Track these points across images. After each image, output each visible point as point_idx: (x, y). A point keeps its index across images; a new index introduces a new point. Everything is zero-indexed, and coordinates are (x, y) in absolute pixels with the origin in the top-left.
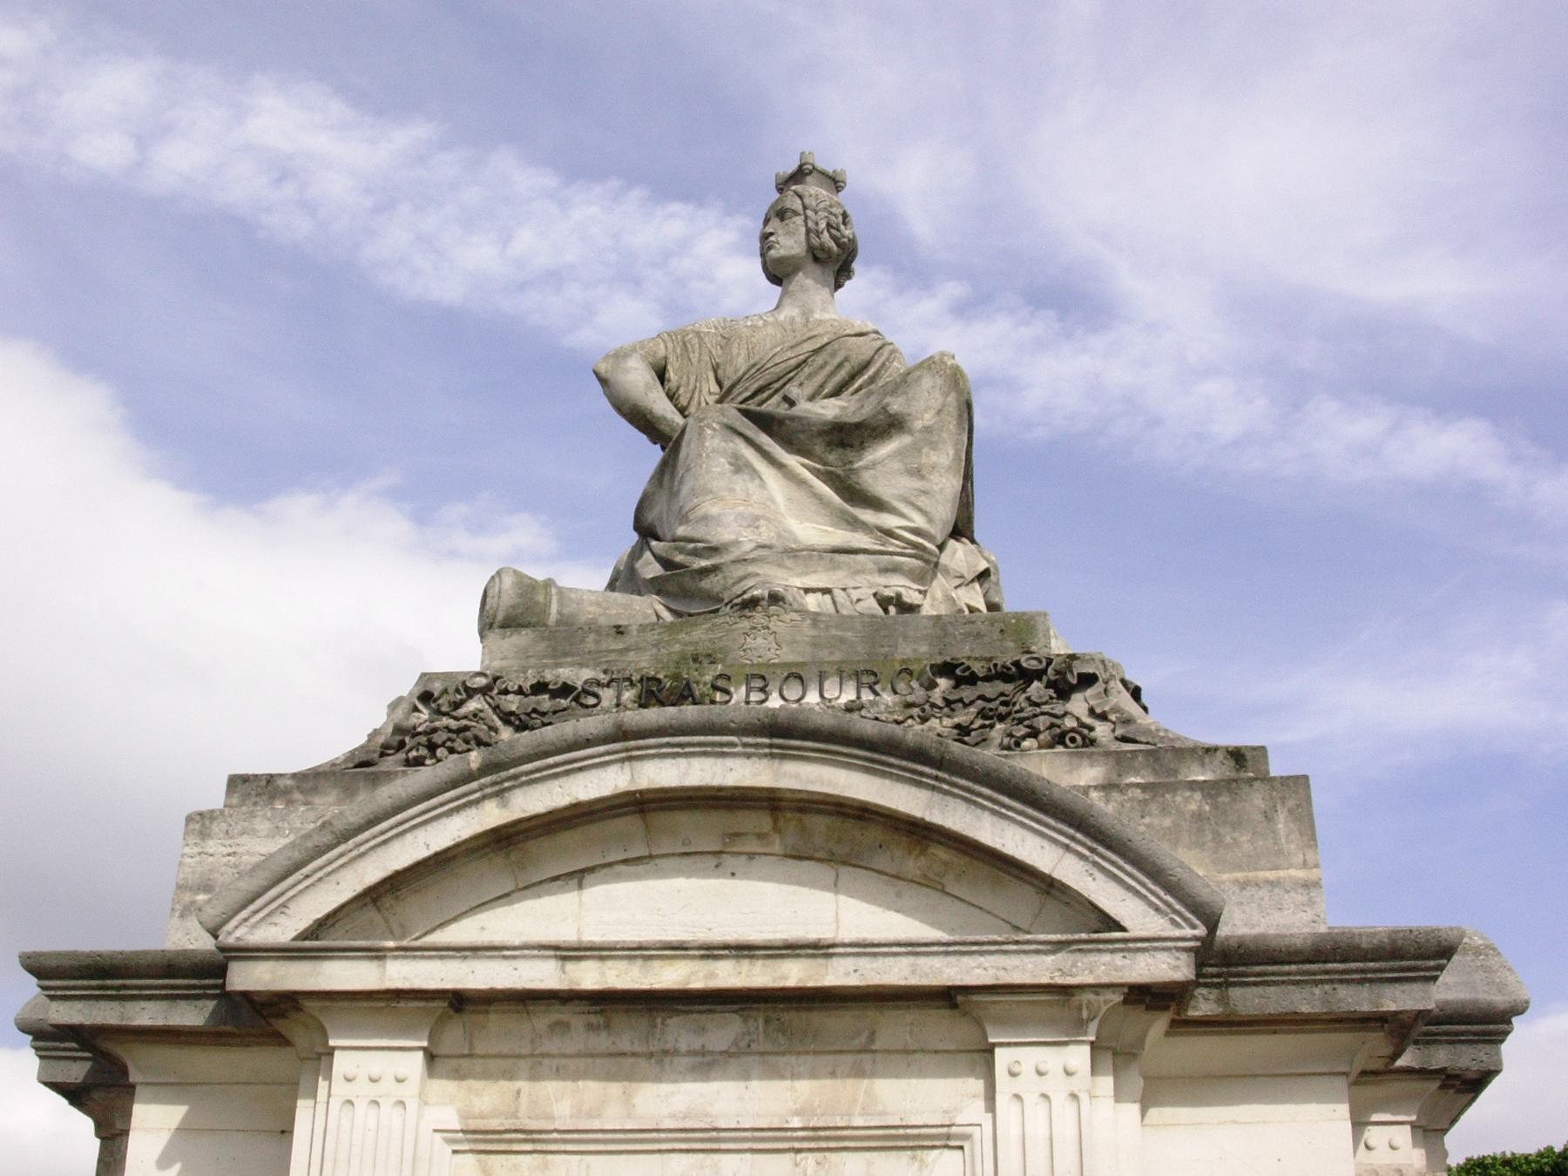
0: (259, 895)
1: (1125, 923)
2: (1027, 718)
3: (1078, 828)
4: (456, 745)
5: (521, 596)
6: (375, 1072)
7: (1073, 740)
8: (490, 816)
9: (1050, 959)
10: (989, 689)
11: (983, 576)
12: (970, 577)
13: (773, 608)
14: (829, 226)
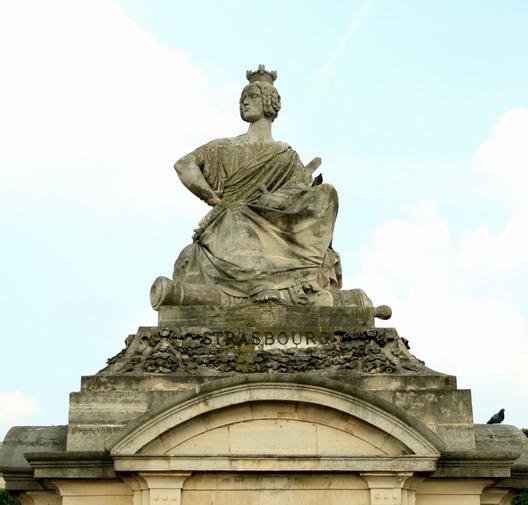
0: (124, 438)
1: (415, 451)
3: (401, 419)
6: (165, 497)
8: (202, 409)
9: (390, 462)
10: (357, 344)
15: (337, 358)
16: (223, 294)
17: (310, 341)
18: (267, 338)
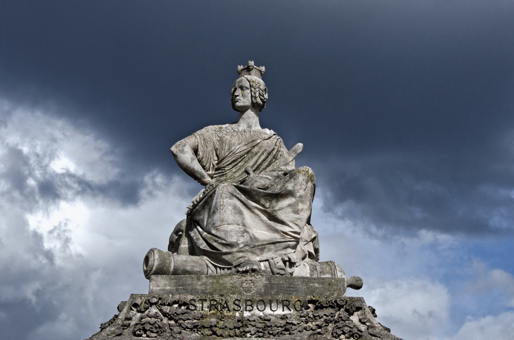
2: (342, 327)
4: (153, 330)
5: (161, 260)
7: (356, 337)
10: (330, 311)
11: (313, 240)
12: (309, 240)
13: (253, 274)
14: (259, 94)
15: (310, 324)
16: (210, 265)
17: (285, 308)
18: (246, 305)
